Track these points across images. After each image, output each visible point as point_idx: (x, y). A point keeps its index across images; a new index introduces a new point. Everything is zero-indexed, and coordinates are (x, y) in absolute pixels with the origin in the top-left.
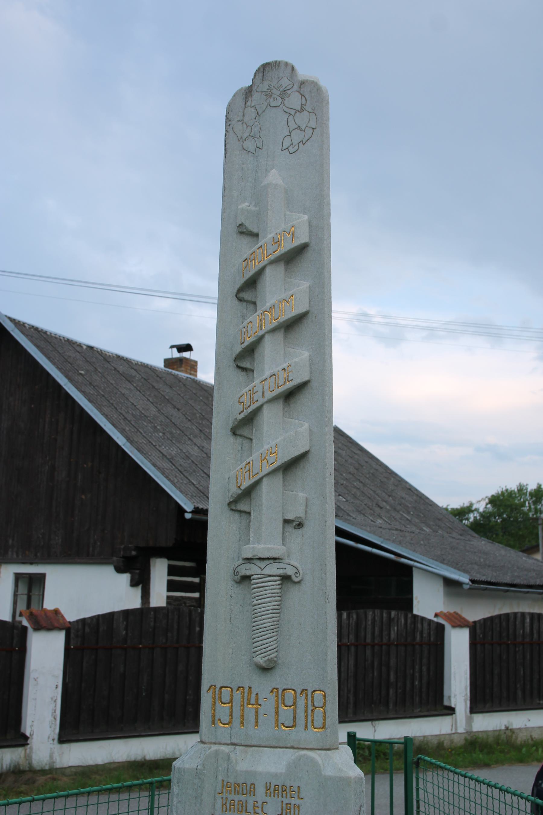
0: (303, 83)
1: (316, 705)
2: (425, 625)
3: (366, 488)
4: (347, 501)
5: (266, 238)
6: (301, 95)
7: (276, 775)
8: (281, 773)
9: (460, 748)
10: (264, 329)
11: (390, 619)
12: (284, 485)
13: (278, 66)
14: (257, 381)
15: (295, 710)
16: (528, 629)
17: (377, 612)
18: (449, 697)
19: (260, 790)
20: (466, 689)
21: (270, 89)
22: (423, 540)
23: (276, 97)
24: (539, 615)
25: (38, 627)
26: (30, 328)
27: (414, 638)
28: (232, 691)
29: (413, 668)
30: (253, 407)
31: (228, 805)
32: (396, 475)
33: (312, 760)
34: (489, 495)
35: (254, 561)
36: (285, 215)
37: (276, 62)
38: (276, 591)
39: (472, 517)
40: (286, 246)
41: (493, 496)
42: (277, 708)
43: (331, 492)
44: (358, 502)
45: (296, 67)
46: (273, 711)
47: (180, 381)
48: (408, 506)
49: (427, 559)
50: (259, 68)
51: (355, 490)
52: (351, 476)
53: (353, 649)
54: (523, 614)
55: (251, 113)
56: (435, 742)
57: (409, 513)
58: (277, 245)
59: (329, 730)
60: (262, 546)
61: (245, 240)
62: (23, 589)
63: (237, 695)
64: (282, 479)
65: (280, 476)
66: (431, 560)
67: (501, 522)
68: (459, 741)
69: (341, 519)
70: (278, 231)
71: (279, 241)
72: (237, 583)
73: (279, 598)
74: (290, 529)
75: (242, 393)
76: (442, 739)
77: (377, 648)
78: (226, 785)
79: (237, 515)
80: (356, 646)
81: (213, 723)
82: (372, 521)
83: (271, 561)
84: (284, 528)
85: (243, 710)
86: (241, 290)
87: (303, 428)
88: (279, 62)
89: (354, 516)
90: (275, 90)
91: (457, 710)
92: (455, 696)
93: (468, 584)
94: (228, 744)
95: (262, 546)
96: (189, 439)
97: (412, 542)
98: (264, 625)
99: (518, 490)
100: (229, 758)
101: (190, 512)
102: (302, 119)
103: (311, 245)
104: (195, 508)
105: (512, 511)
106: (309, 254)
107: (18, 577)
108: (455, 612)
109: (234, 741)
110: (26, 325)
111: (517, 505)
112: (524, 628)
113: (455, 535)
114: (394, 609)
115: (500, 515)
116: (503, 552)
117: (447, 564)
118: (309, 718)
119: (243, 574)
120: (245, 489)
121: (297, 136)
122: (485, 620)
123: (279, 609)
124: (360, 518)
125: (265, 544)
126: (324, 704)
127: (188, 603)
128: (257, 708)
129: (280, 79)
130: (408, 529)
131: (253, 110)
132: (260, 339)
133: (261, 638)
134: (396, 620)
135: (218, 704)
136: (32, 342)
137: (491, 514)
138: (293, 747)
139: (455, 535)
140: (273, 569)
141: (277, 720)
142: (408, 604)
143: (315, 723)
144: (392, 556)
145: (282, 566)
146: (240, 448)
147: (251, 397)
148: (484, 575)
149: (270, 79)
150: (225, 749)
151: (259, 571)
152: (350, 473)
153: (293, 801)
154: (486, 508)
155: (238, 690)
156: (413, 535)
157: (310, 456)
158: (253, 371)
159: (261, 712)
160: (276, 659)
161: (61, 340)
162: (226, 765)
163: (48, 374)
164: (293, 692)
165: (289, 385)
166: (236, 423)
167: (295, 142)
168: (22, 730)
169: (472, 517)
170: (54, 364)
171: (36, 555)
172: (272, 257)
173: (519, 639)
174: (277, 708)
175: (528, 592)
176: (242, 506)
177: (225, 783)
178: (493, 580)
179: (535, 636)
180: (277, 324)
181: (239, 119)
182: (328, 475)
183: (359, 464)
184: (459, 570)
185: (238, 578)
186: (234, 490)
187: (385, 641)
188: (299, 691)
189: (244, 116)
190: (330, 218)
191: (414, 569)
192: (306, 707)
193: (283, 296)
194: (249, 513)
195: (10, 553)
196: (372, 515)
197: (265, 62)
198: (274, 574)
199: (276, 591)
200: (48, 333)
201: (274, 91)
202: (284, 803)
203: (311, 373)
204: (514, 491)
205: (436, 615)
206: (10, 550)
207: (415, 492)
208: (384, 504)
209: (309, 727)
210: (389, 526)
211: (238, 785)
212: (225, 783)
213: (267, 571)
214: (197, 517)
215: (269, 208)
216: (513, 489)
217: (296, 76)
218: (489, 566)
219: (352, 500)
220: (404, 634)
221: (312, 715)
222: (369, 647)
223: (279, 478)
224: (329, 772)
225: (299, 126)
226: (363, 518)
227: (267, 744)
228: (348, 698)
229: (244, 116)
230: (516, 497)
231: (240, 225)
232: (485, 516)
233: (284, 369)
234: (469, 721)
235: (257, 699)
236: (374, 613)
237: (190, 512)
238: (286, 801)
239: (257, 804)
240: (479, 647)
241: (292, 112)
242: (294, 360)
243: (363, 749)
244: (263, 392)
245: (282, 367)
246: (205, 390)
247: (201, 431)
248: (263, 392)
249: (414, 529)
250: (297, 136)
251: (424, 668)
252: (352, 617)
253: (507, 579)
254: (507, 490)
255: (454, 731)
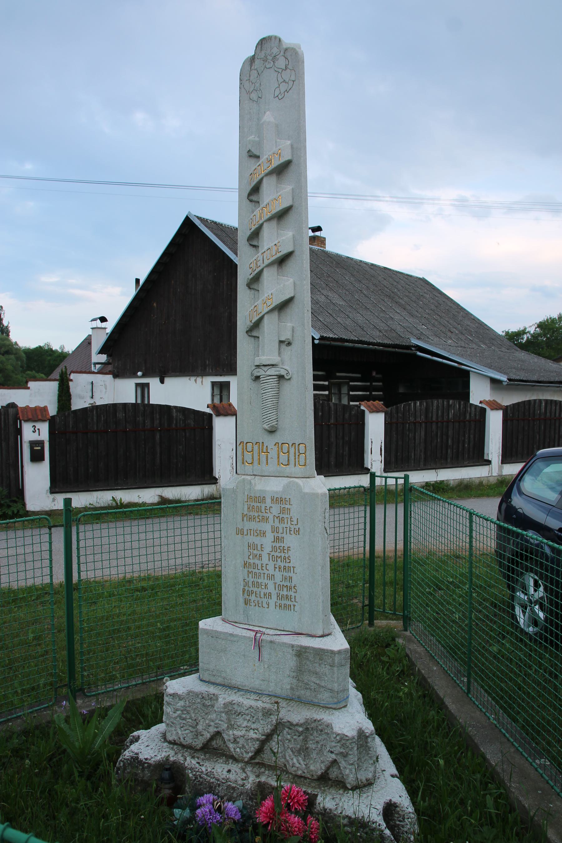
0: (286, 50)
1: (301, 452)
2: (473, 409)
3: (442, 320)
4: (428, 328)
5: (263, 159)
6: (285, 58)
7: (277, 492)
8: (279, 491)
9: (494, 485)
10: (263, 220)
11: (449, 406)
12: (279, 319)
13: (271, 40)
14: (260, 253)
15: (289, 455)
16: (543, 410)
17: (440, 401)
18: (488, 454)
19: (268, 500)
20: (499, 449)
21: (266, 56)
22: (479, 353)
23: (270, 61)
24: (561, 401)
25: (219, 414)
26: (211, 223)
27: (465, 417)
28: (289, 446)
29: (464, 436)
30: (257, 270)
31: (251, 508)
32: (465, 310)
33: (297, 484)
34: (538, 322)
35: (261, 367)
36: (276, 142)
37: (269, 36)
38: (274, 385)
39: (525, 337)
40: (275, 163)
41: (540, 322)
42: (279, 454)
43: (308, 322)
44: (436, 329)
45: (283, 38)
46: (276, 456)
47: (313, 252)
48: (471, 331)
49: (479, 366)
50: (259, 42)
51: (434, 321)
52: (432, 312)
53: (423, 425)
54: (540, 401)
55: (254, 73)
56: (477, 481)
57: (471, 335)
58: (269, 163)
59: (308, 467)
60: (265, 357)
61: (253, 160)
62: (217, 391)
63: (256, 447)
64: (277, 316)
65: (276, 313)
66: (482, 367)
67: (546, 340)
68: (493, 481)
69: (422, 341)
70: (270, 153)
71: (271, 160)
72: (254, 380)
73: (277, 389)
74: (283, 346)
75: (251, 262)
76: (482, 480)
77: (439, 424)
78: (250, 498)
79: (252, 339)
80: (426, 423)
81: (243, 463)
82: (444, 341)
83: (271, 367)
84: (280, 346)
85: (259, 456)
86: (250, 194)
87: (289, 282)
88: (271, 37)
89: (432, 339)
90: (269, 56)
91: (493, 462)
92: (492, 453)
93: (506, 382)
94: (251, 475)
95: (265, 357)
96: (319, 291)
97: (471, 355)
98: (268, 406)
99: (558, 318)
100: (251, 483)
101: (318, 339)
102: (286, 75)
103: (293, 161)
104: (321, 336)
105: (553, 332)
106: (292, 168)
107: (213, 384)
108: (494, 400)
109: (255, 473)
110: (209, 221)
111: (557, 328)
112: (540, 409)
113: (503, 349)
114: (451, 399)
115: (545, 335)
116: (536, 360)
117: (493, 369)
118: (297, 460)
119: (256, 375)
120: (254, 323)
121: (283, 87)
122: (514, 405)
123: (278, 396)
124: (436, 339)
125: (267, 356)
126: (305, 452)
127: (321, 398)
128: (267, 455)
129: (271, 48)
130: (470, 346)
131: (256, 72)
132: (261, 226)
133: (266, 414)
134: (453, 406)
135: (245, 452)
136: (212, 232)
137: (539, 335)
138: (288, 477)
139: (503, 349)
140: (272, 371)
141: (279, 461)
142: (466, 395)
143: (300, 463)
144: (456, 365)
145: (278, 369)
146: (253, 297)
147: (256, 264)
148: (519, 375)
149: (266, 49)
150: (249, 478)
151: (264, 373)
152: (431, 309)
153: (287, 506)
154: (535, 330)
155: (256, 444)
156: (472, 350)
157: (295, 300)
158: (258, 247)
159: (269, 457)
160: (276, 426)
161: (232, 229)
162: (249, 487)
163: (224, 253)
164: (287, 445)
165: (279, 255)
166: (249, 281)
167: (282, 92)
168: (214, 475)
169: (525, 337)
170: (227, 245)
171: (223, 370)
172: (266, 171)
173: (537, 417)
174: (279, 454)
175: (549, 386)
176: (255, 333)
177: (249, 497)
178: (525, 379)
179: (548, 414)
180: (270, 215)
181: (247, 79)
182: (306, 311)
183: (438, 303)
184: (501, 372)
185: (253, 377)
186: (249, 324)
187: (445, 419)
188: (291, 444)
189: (250, 76)
190: (306, 141)
191: (470, 372)
192: (295, 454)
193: (274, 197)
194: (259, 337)
195: (207, 369)
196: (445, 337)
197: (262, 38)
198: (273, 374)
199: (274, 385)
200: (223, 225)
201: (269, 57)
202: (282, 507)
203: (294, 246)
204: (555, 318)
205: (481, 402)
206: (207, 367)
207: (478, 321)
208: (454, 330)
209: (297, 465)
210: (456, 345)
211: (256, 497)
212: (249, 497)
213: (268, 373)
214: (323, 342)
215: (265, 138)
216: (554, 317)
217: (283, 44)
218: (523, 370)
219: (432, 328)
220: (458, 415)
221: (299, 458)
222: (435, 423)
223: (275, 315)
224: (306, 490)
225: (284, 80)
226: (438, 340)
227: (273, 475)
228: (420, 455)
229: (250, 76)
230: (557, 323)
231: (249, 151)
232: (535, 336)
233: (276, 245)
234: (500, 469)
235: (267, 449)
236: (438, 401)
237: (318, 339)
238: (282, 506)
239: (266, 508)
240: (509, 422)
241: (280, 71)
242: (282, 239)
243: (429, 486)
244: (263, 260)
245: (274, 243)
246: (331, 257)
247: (327, 285)
248: (263, 260)
249: (474, 346)
250: (283, 87)
251: (472, 436)
252: (423, 405)
253: (535, 378)
254: (550, 318)
255: (490, 475)
